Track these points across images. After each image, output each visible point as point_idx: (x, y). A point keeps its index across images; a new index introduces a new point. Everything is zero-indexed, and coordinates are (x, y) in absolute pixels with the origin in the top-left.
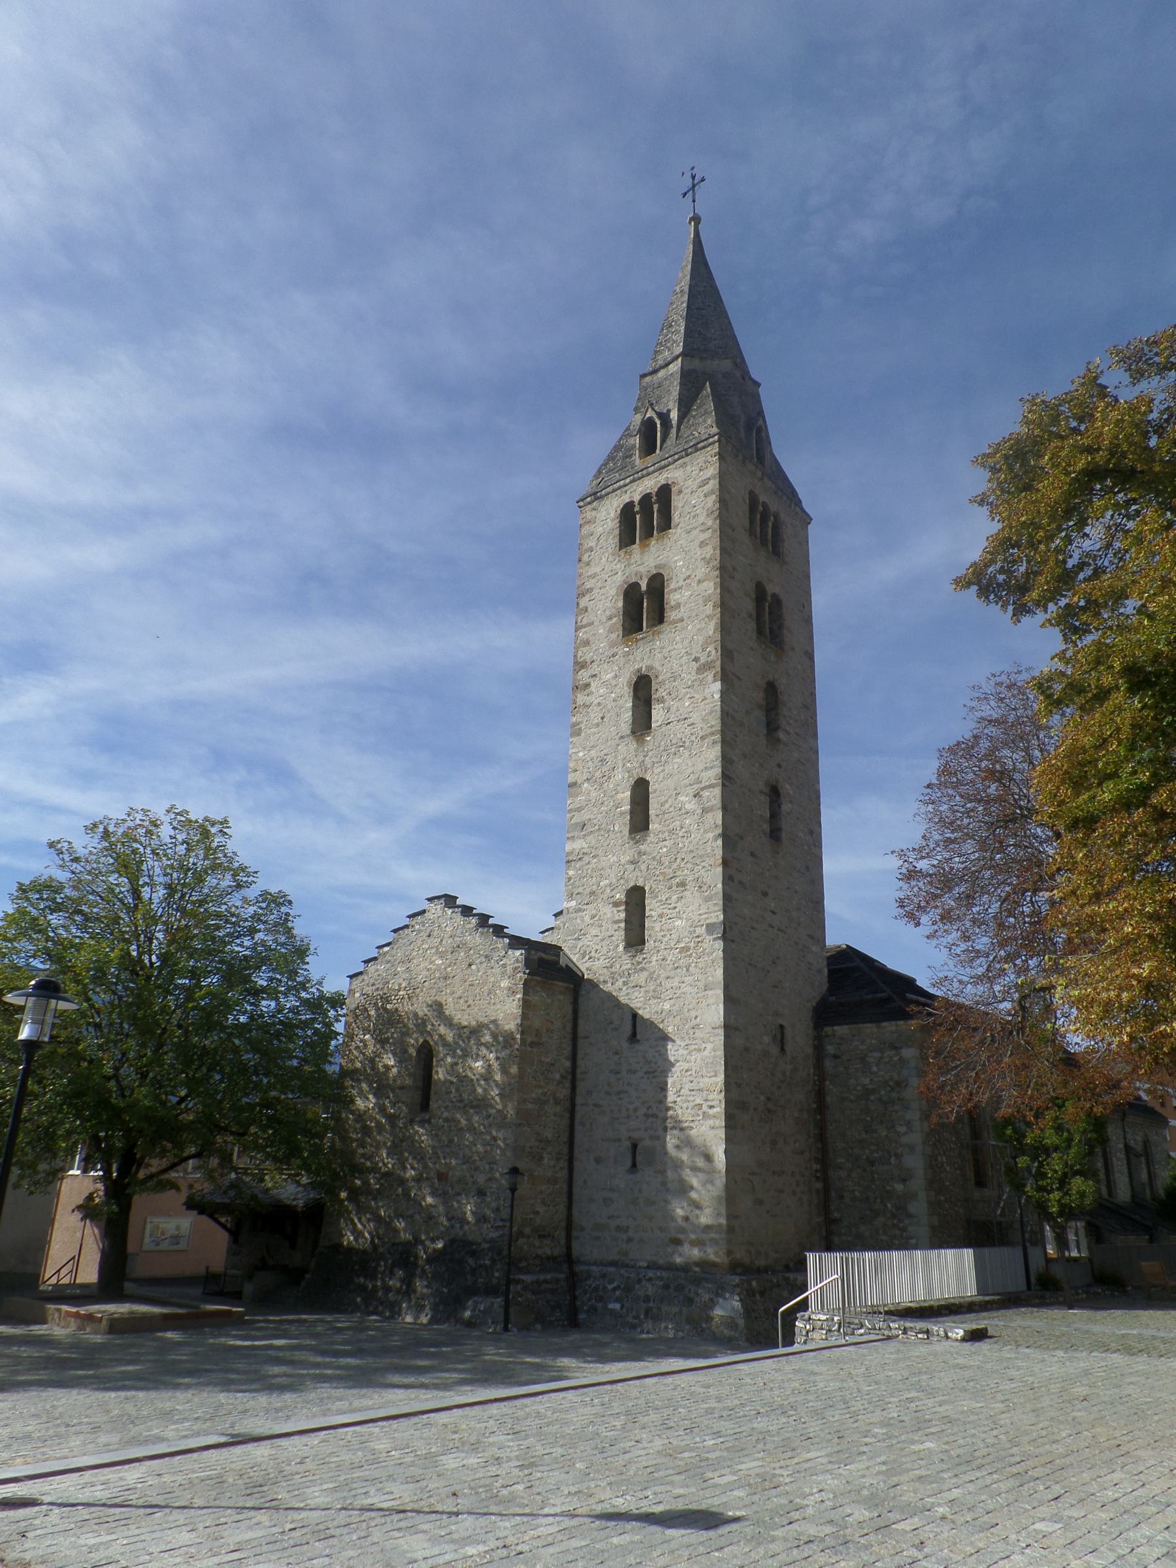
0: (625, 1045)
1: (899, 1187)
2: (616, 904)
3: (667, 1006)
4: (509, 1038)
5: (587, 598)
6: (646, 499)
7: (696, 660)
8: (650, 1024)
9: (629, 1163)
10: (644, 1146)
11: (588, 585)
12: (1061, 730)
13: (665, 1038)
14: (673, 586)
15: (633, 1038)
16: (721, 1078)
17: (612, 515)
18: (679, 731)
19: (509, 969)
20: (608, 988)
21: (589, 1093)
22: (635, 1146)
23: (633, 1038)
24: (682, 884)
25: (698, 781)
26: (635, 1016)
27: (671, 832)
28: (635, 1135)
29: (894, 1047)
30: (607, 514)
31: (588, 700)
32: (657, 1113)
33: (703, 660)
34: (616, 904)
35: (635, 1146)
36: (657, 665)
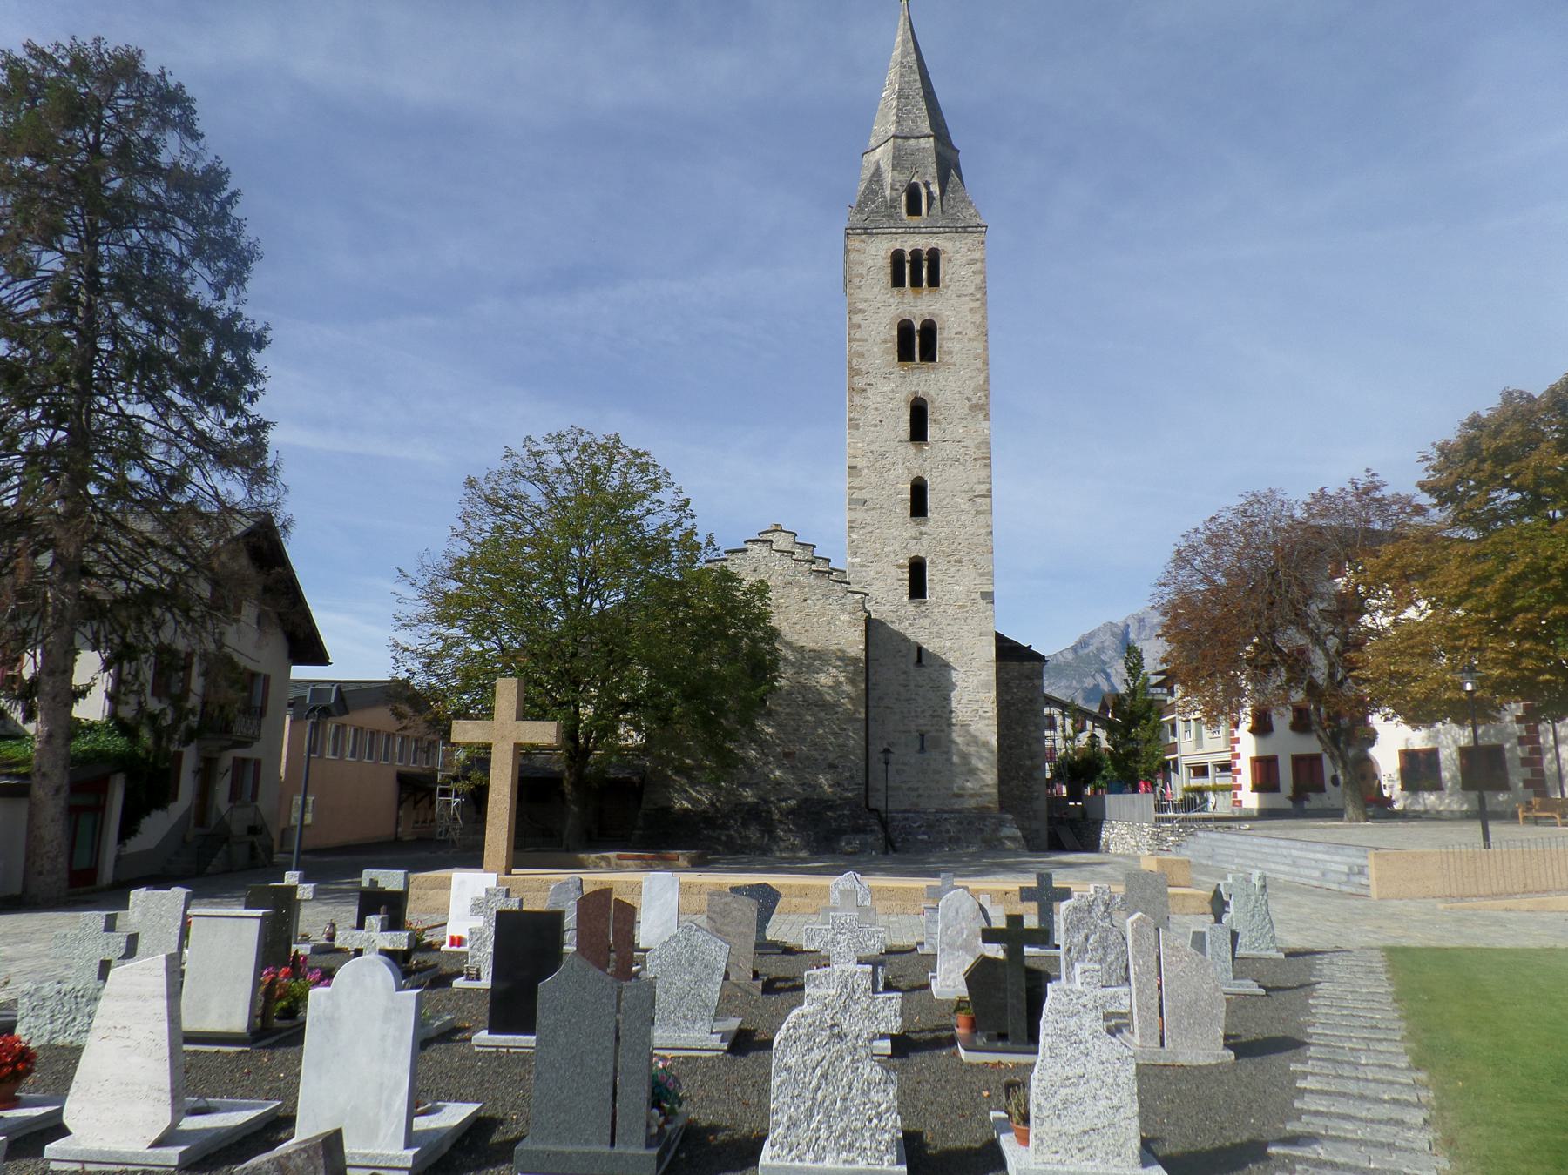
0: (912, 668)
1: (1028, 763)
2: (899, 567)
3: (949, 644)
4: (855, 660)
5: (860, 316)
6: (916, 254)
7: (968, 399)
8: (935, 657)
9: (918, 746)
10: (934, 732)
11: (861, 306)
12: (1230, 515)
13: (947, 665)
14: (945, 335)
15: (919, 660)
16: (994, 694)
17: (883, 253)
18: (951, 450)
19: (849, 608)
20: (895, 627)
21: (881, 698)
22: (922, 735)
23: (919, 660)
24: (960, 561)
25: (972, 490)
26: (920, 649)
27: (949, 523)
28: (924, 729)
29: (1028, 677)
30: (877, 252)
31: (867, 403)
32: (943, 713)
33: (975, 401)
34: (899, 567)
35: (922, 735)
36: (932, 393)
